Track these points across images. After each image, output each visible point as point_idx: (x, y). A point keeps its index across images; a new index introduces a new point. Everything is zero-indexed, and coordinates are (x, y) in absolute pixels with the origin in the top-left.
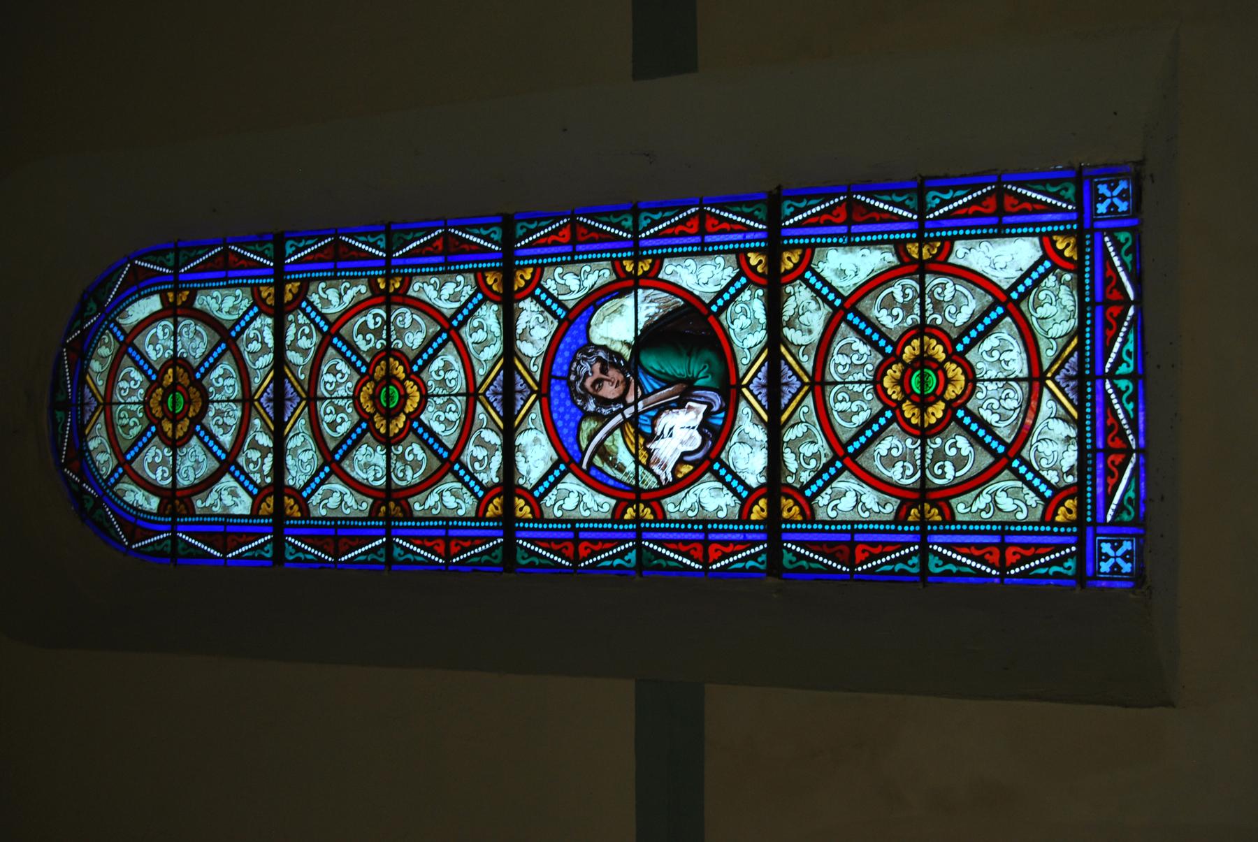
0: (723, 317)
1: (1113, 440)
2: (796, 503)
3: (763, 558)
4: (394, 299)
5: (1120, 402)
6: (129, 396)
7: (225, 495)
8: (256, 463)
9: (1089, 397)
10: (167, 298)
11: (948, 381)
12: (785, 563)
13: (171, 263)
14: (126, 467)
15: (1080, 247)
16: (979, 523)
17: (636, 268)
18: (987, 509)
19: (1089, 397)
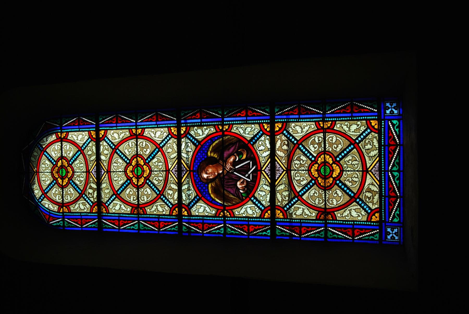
0: (254, 146)
1: (391, 193)
2: (281, 212)
3: (176, 227)
4: (139, 137)
5: (394, 180)
6: (46, 170)
7: (81, 205)
8: (91, 194)
10: (58, 135)
11: (317, 170)
12: (183, 230)
13: (59, 123)
14: (45, 194)
15: (380, 124)
16: (153, 215)
17: (136, 132)
18: (155, 211)
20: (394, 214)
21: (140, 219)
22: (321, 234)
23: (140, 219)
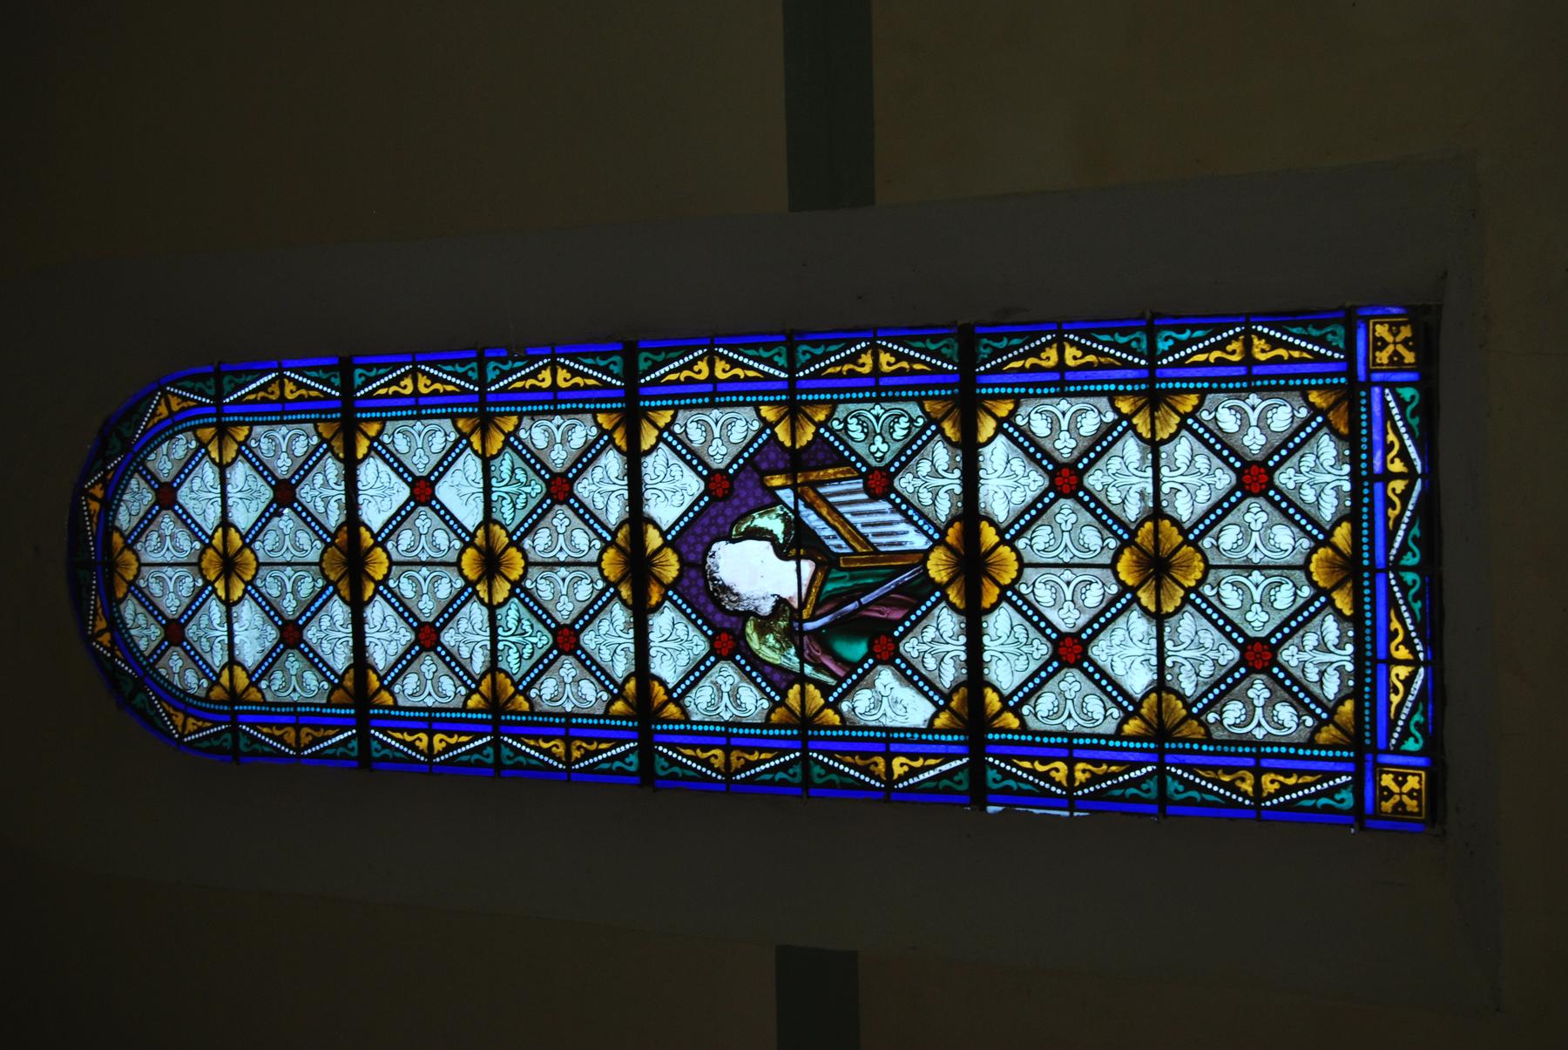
9: (1366, 583)
13: (212, 392)
19: (1366, 500)
20: (1407, 722)
21: (1168, 758)
22: (956, 778)
23: (1168, 758)
